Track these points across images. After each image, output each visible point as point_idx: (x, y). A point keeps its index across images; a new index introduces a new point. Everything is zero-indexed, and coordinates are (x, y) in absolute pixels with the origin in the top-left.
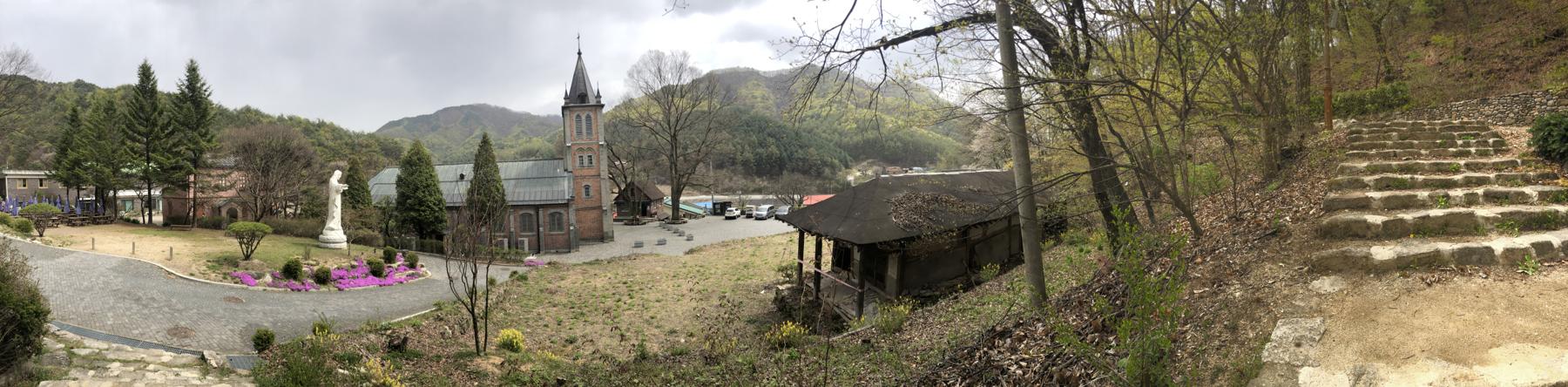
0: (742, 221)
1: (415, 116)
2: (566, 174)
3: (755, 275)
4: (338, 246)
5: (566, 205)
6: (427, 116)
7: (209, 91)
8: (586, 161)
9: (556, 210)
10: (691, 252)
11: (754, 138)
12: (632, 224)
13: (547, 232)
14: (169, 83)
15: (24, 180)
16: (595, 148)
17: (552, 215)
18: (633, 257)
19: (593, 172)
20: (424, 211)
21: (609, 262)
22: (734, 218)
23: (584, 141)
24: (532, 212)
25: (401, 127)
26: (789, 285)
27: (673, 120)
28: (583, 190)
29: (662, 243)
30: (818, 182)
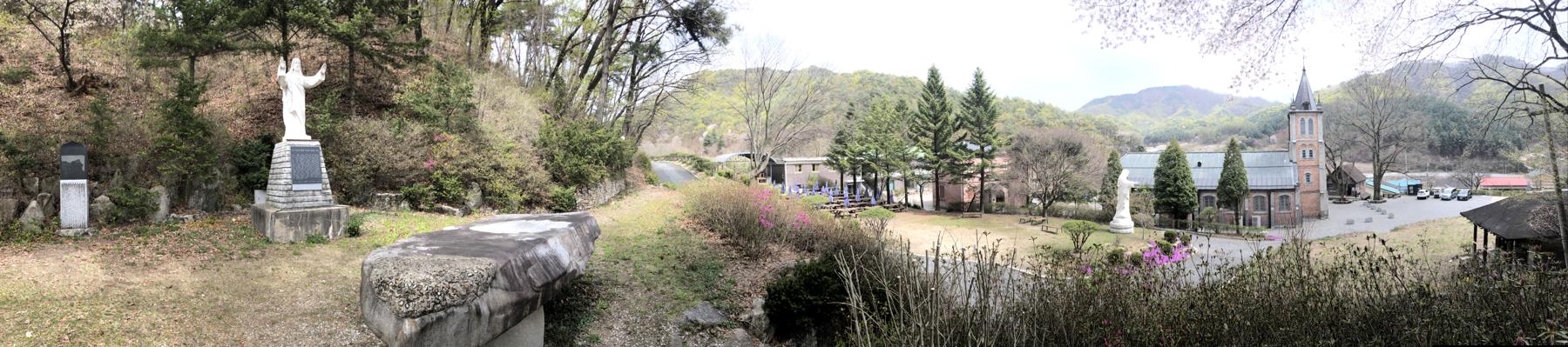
0: (1431, 200)
1: (1119, 94)
2: (1291, 164)
3: (1444, 249)
4: (1128, 231)
5: (1293, 190)
6: (1131, 95)
7: (993, 94)
8: (1308, 154)
9: (1286, 192)
10: (1396, 229)
11: (1439, 123)
12: (1340, 203)
13: (1277, 211)
14: (957, 83)
15: (800, 166)
16: (1315, 144)
17: (1282, 197)
18: (1354, 235)
19: (1313, 163)
20: (1182, 197)
21: (1337, 239)
22: (1424, 198)
23: (1307, 138)
24: (1265, 195)
25: (1104, 104)
26: (1468, 257)
27: (1376, 121)
28: (1305, 177)
29: (1369, 221)
30: (1494, 162)
